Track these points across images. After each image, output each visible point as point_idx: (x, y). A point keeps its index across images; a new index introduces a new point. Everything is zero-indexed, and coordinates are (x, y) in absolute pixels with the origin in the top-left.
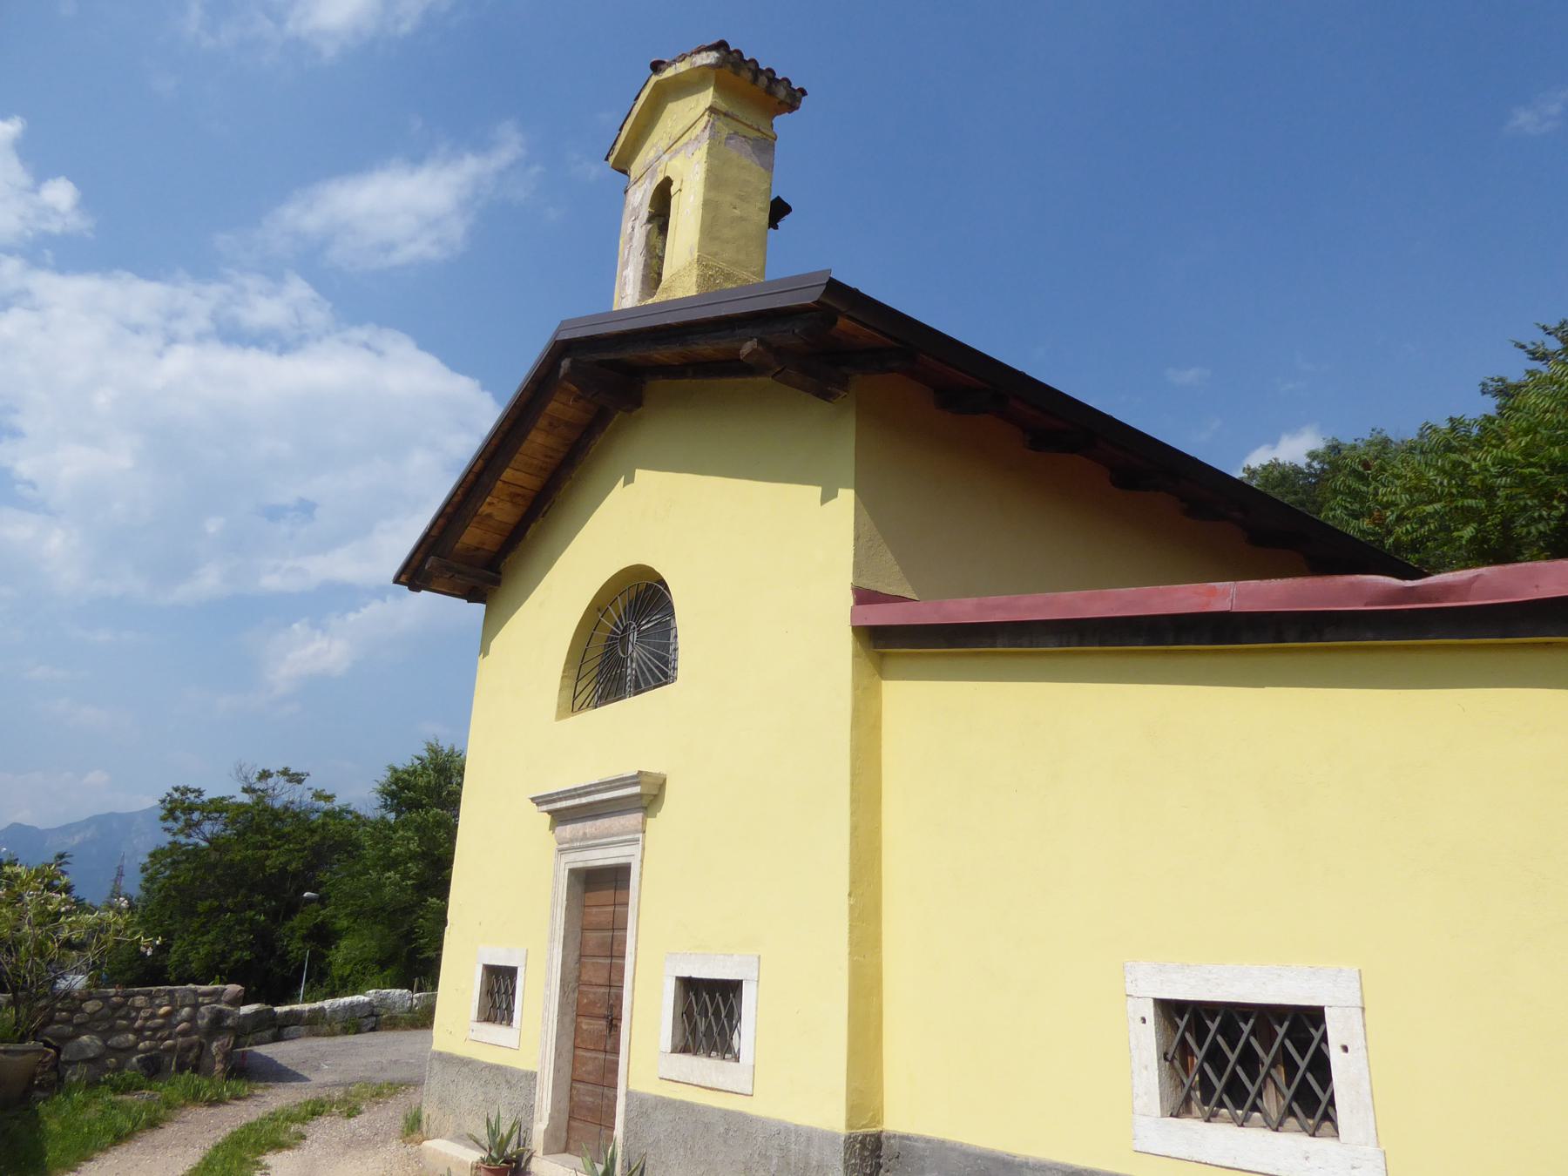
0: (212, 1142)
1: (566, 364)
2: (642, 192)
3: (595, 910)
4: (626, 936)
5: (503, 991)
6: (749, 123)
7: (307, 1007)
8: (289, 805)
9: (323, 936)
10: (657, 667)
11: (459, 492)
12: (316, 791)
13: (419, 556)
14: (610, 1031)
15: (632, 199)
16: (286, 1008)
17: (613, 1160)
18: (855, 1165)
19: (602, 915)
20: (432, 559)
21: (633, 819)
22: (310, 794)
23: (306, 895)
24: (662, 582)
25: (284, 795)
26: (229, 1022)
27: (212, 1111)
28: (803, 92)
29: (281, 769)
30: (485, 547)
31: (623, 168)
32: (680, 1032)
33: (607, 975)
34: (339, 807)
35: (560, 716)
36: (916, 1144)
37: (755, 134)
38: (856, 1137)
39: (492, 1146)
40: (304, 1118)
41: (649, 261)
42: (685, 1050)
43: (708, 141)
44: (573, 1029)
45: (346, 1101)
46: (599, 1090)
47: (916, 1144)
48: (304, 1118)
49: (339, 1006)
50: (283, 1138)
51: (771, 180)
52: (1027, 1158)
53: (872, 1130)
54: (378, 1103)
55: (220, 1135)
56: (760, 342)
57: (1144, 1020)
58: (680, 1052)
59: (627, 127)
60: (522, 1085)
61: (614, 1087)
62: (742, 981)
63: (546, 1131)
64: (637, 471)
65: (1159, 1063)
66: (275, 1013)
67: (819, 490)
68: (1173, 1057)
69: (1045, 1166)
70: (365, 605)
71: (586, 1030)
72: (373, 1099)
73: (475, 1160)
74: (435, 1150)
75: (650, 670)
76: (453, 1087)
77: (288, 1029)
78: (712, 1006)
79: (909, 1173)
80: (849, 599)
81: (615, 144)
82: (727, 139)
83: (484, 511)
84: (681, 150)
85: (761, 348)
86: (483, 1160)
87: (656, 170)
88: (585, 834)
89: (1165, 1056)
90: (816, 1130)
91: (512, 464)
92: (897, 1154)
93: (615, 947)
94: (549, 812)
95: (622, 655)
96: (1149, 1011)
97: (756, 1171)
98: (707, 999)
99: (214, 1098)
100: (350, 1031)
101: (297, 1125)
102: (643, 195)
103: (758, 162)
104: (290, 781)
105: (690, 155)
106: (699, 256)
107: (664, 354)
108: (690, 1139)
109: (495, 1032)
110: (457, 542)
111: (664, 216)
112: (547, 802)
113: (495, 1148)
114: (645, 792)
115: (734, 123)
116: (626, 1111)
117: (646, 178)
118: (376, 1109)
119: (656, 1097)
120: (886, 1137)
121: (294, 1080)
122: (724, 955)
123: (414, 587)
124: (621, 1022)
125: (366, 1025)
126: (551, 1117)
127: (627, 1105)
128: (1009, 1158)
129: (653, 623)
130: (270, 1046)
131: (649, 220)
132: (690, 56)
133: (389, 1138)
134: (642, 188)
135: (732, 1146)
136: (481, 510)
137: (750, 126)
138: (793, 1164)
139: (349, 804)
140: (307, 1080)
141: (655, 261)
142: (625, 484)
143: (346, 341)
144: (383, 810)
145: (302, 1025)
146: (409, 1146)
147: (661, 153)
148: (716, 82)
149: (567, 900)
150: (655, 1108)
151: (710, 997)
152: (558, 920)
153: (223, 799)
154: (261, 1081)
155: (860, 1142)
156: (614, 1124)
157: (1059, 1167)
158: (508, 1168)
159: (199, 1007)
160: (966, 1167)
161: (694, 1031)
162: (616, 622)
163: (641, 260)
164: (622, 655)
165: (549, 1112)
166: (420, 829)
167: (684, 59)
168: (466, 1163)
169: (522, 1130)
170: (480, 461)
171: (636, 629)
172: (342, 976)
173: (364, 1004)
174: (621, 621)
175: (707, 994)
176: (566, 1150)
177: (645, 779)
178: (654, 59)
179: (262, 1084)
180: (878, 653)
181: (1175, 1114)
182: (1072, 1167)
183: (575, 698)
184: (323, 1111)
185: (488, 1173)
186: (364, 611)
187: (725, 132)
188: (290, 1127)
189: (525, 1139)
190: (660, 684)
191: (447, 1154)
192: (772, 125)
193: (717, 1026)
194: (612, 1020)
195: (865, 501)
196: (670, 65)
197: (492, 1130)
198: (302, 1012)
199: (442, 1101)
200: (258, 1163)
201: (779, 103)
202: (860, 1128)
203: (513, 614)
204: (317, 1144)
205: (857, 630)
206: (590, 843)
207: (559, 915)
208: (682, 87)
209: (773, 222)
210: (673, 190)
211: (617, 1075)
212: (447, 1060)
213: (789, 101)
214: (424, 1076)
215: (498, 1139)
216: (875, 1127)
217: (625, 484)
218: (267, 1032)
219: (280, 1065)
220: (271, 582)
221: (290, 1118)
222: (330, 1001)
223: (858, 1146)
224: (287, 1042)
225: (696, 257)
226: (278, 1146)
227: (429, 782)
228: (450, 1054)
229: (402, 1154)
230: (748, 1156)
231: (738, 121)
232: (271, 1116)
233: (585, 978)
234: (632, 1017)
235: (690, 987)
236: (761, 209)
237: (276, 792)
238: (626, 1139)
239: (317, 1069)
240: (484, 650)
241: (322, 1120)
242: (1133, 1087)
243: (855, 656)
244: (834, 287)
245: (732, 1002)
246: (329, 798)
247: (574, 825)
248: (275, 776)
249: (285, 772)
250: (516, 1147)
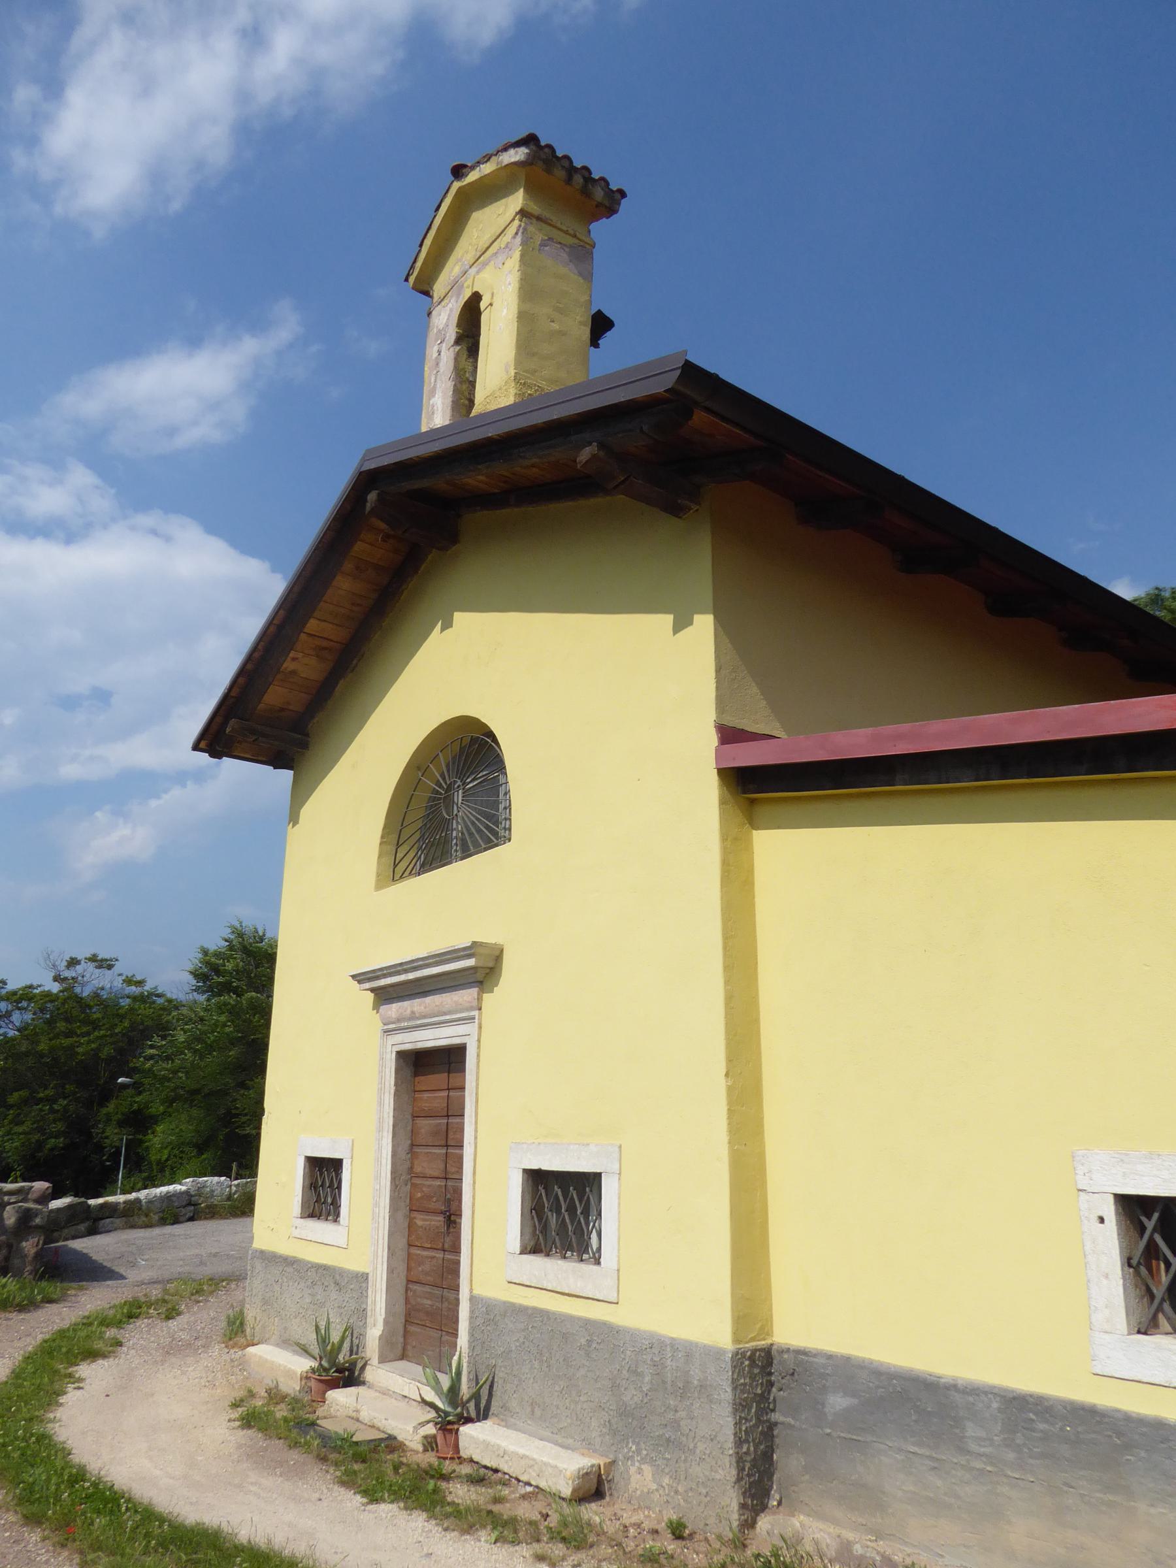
0: (22, 1352)
1: (372, 496)
2: (448, 312)
3: (426, 1095)
4: (464, 1123)
5: (328, 1185)
6: (564, 228)
7: (120, 1198)
8: (99, 991)
9: (140, 1122)
10: (487, 827)
11: (260, 647)
12: (127, 977)
13: (219, 719)
14: (448, 1227)
15: (437, 321)
16: (100, 1201)
17: (459, 1373)
18: (744, 1385)
19: (434, 1100)
20: (233, 722)
21: (467, 996)
22: (120, 979)
23: (120, 1080)
24: (491, 735)
25: (94, 981)
26: (38, 1221)
27: (22, 1316)
28: (622, 194)
29: (88, 956)
30: (291, 707)
31: (425, 288)
32: (529, 1230)
33: (442, 1166)
34: (147, 991)
35: (380, 885)
36: (815, 1360)
37: (570, 241)
38: (744, 1354)
39: (323, 1355)
40: (120, 1322)
41: (459, 386)
42: (535, 1250)
43: (521, 248)
44: (407, 1224)
45: (165, 1301)
46: (438, 1292)
47: (815, 1360)
48: (120, 1322)
49: (155, 1197)
50: (98, 1345)
51: (591, 291)
52: (955, 1379)
53: (762, 1343)
54: (199, 1302)
55: (31, 1344)
56: (602, 446)
57: (1102, 1220)
58: (530, 1253)
59: (428, 242)
60: (352, 1286)
61: (456, 1289)
62: (600, 1174)
63: (380, 1338)
64: (456, 614)
65: (1123, 1270)
66: (89, 1206)
67: (669, 619)
68: (1139, 1263)
69: (978, 1389)
70: (166, 791)
71: (422, 1227)
72: (193, 1298)
73: (305, 1370)
74: (260, 1357)
75: (479, 831)
76: (277, 1288)
77: (103, 1221)
78: (565, 1202)
79: (806, 1392)
80: (713, 739)
81: (415, 262)
82: (541, 245)
83: (286, 669)
84: (490, 261)
85: (601, 453)
86: (313, 1370)
87: (463, 285)
88: (413, 1012)
89: (1128, 1262)
90: (697, 1345)
91: (317, 614)
92: (792, 1371)
93: (451, 1135)
94: (372, 990)
95: (446, 816)
96: (1109, 1210)
97: (626, 1389)
98: (560, 1193)
99: (25, 1302)
100: (168, 1222)
101: (112, 1330)
102: (449, 316)
103: (576, 272)
104: (100, 967)
105: (501, 266)
106: (516, 373)
107: (477, 479)
108: (545, 1350)
109: (319, 1229)
110: (260, 703)
111: (473, 337)
112: (370, 980)
113: (325, 1356)
114: (480, 965)
115: (549, 228)
116: (471, 1318)
117: (452, 297)
118: (196, 1309)
119: (505, 1303)
120: (778, 1351)
121: (110, 1279)
123: (215, 753)
124: (461, 1218)
125: (185, 1214)
126: (386, 1322)
127: (472, 1312)
128: (932, 1378)
129: (479, 781)
130: (85, 1240)
131: (458, 341)
132: (496, 155)
133: (211, 1342)
134: (448, 308)
135: (595, 1360)
136: (284, 666)
137: (566, 232)
138: (669, 1383)
139: (156, 987)
140: (122, 1277)
141: (464, 387)
142: (443, 630)
143: (133, 528)
144: (195, 993)
145: (117, 1218)
146: (232, 1351)
147: (467, 267)
148: (526, 181)
149: (396, 1085)
150: (504, 1315)
151: (562, 1192)
152: (386, 1107)
153: (31, 987)
154: (74, 1281)
155: (750, 1358)
156: (457, 1331)
157: (995, 1391)
158: (341, 1377)
159: (5, 1207)
160: (878, 1387)
161: (545, 1228)
162: (438, 781)
163: (450, 385)
164: (446, 816)
165: (383, 1316)
166: (234, 1012)
167: (489, 160)
168: (294, 1373)
169: (355, 1336)
170: (282, 612)
171: (462, 787)
172: (160, 1159)
173: (182, 1193)
174: (444, 779)
175: (559, 1188)
176: (403, 1357)
177: (480, 950)
178: (456, 163)
179: (73, 1285)
180: (749, 799)
181: (1143, 1330)
182: (1013, 1391)
183: (395, 866)
184: (140, 1314)
185: (321, 1385)
186: (166, 797)
187: (539, 237)
188: (105, 1332)
189: (358, 1346)
190: (490, 845)
191: (273, 1362)
192: (589, 232)
193: (572, 1223)
194: (449, 1217)
195: (726, 628)
196: (473, 168)
197: (322, 1337)
198: (117, 1204)
199: (266, 1302)
200: (70, 1376)
201: (597, 206)
202: (747, 1343)
203: (324, 778)
204: (133, 1351)
205: (724, 773)
206: (419, 1022)
207: (387, 1102)
208: (489, 192)
209: (595, 341)
210: (483, 305)
211: (458, 1276)
212: (271, 1258)
213: (607, 203)
214: (246, 1270)
215: (329, 1348)
216: (764, 1339)
217: (443, 630)
218: (82, 1225)
219: (95, 1262)
220: (71, 771)
221: (105, 1322)
222: (146, 1192)
223: (747, 1363)
224: (103, 1235)
225: (513, 374)
226: (92, 1355)
227: (237, 965)
228: (273, 1252)
229: (225, 1361)
230: (616, 1372)
231: (550, 225)
232: (85, 1321)
233: (418, 1169)
234: (473, 1213)
235: (537, 1179)
236: (581, 323)
237: (85, 978)
238: (472, 1347)
239: (133, 1265)
240: (294, 818)
241: (139, 1323)
242: (1089, 1298)
243: (723, 802)
244: (691, 372)
245: (588, 1198)
246: (140, 983)
247: (400, 1004)
248: (82, 962)
249: (93, 959)
250: (348, 1354)
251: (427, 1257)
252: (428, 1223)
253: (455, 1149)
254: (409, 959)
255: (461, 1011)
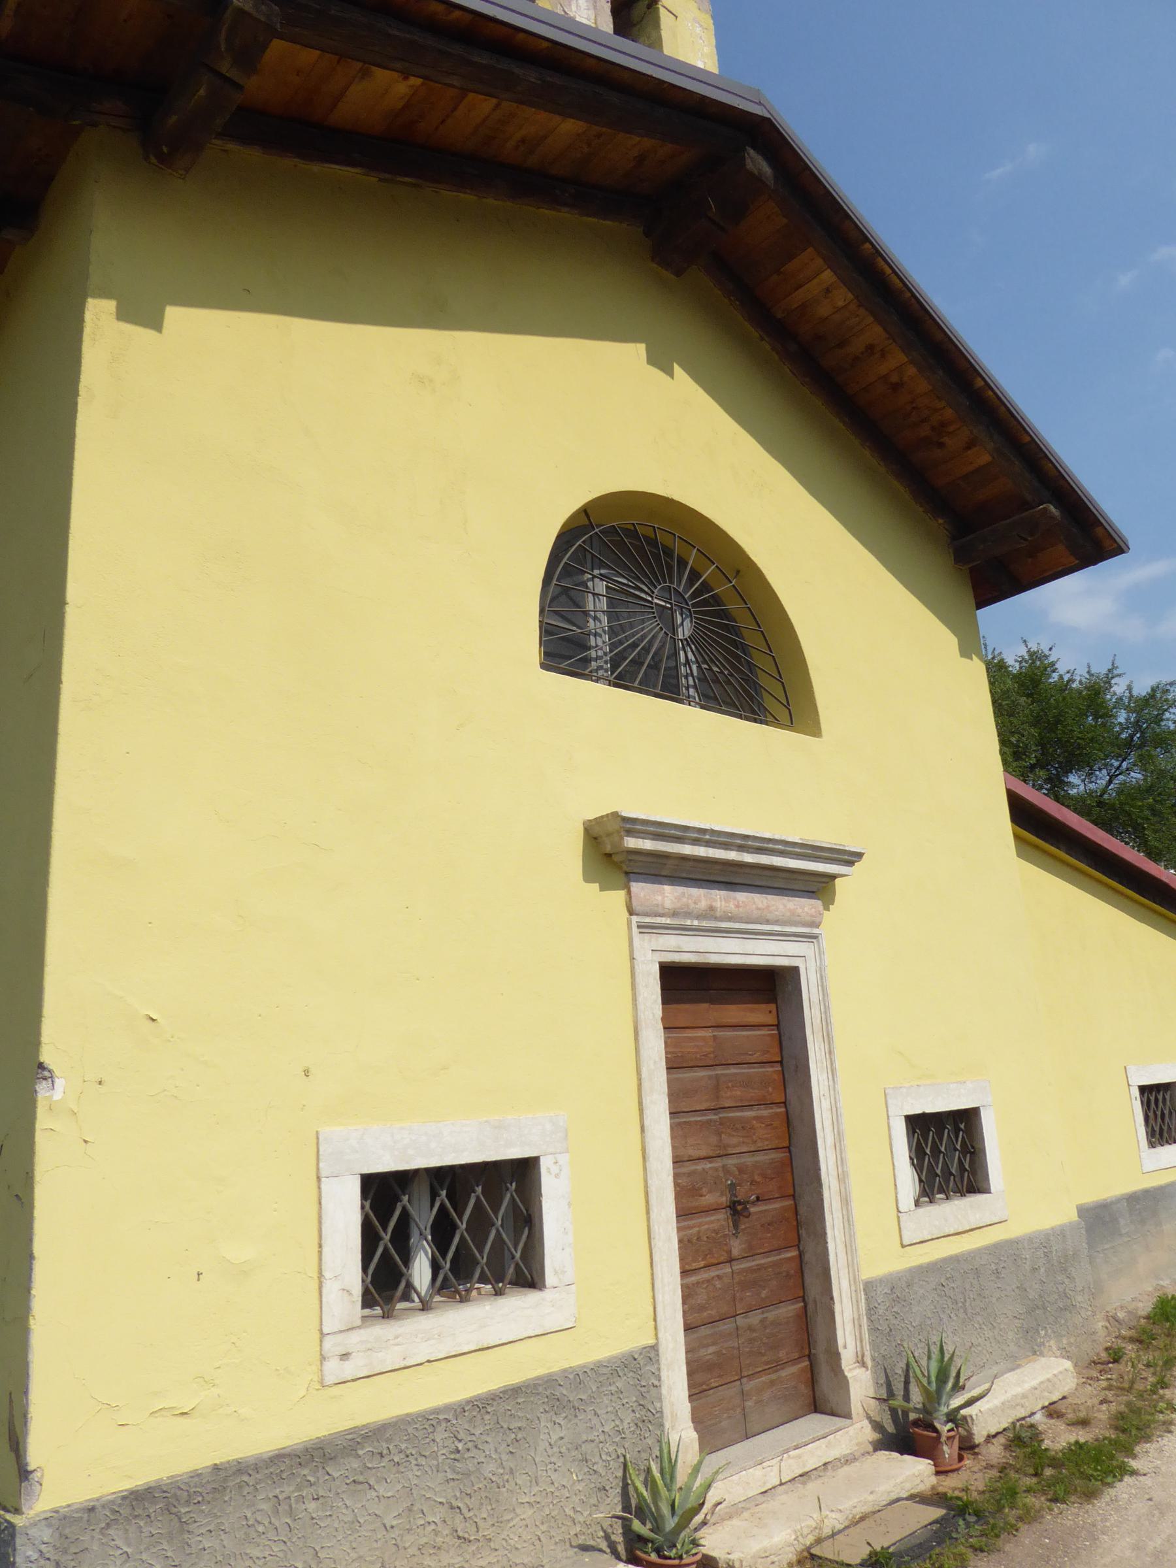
62: (979, 1107)
122: (957, 1083)
170: (545, 44)
235: (919, 1124)
251: (698, 1283)
252: (696, 1229)
253: (734, 1112)
254: (768, 835)
255: (795, 924)
